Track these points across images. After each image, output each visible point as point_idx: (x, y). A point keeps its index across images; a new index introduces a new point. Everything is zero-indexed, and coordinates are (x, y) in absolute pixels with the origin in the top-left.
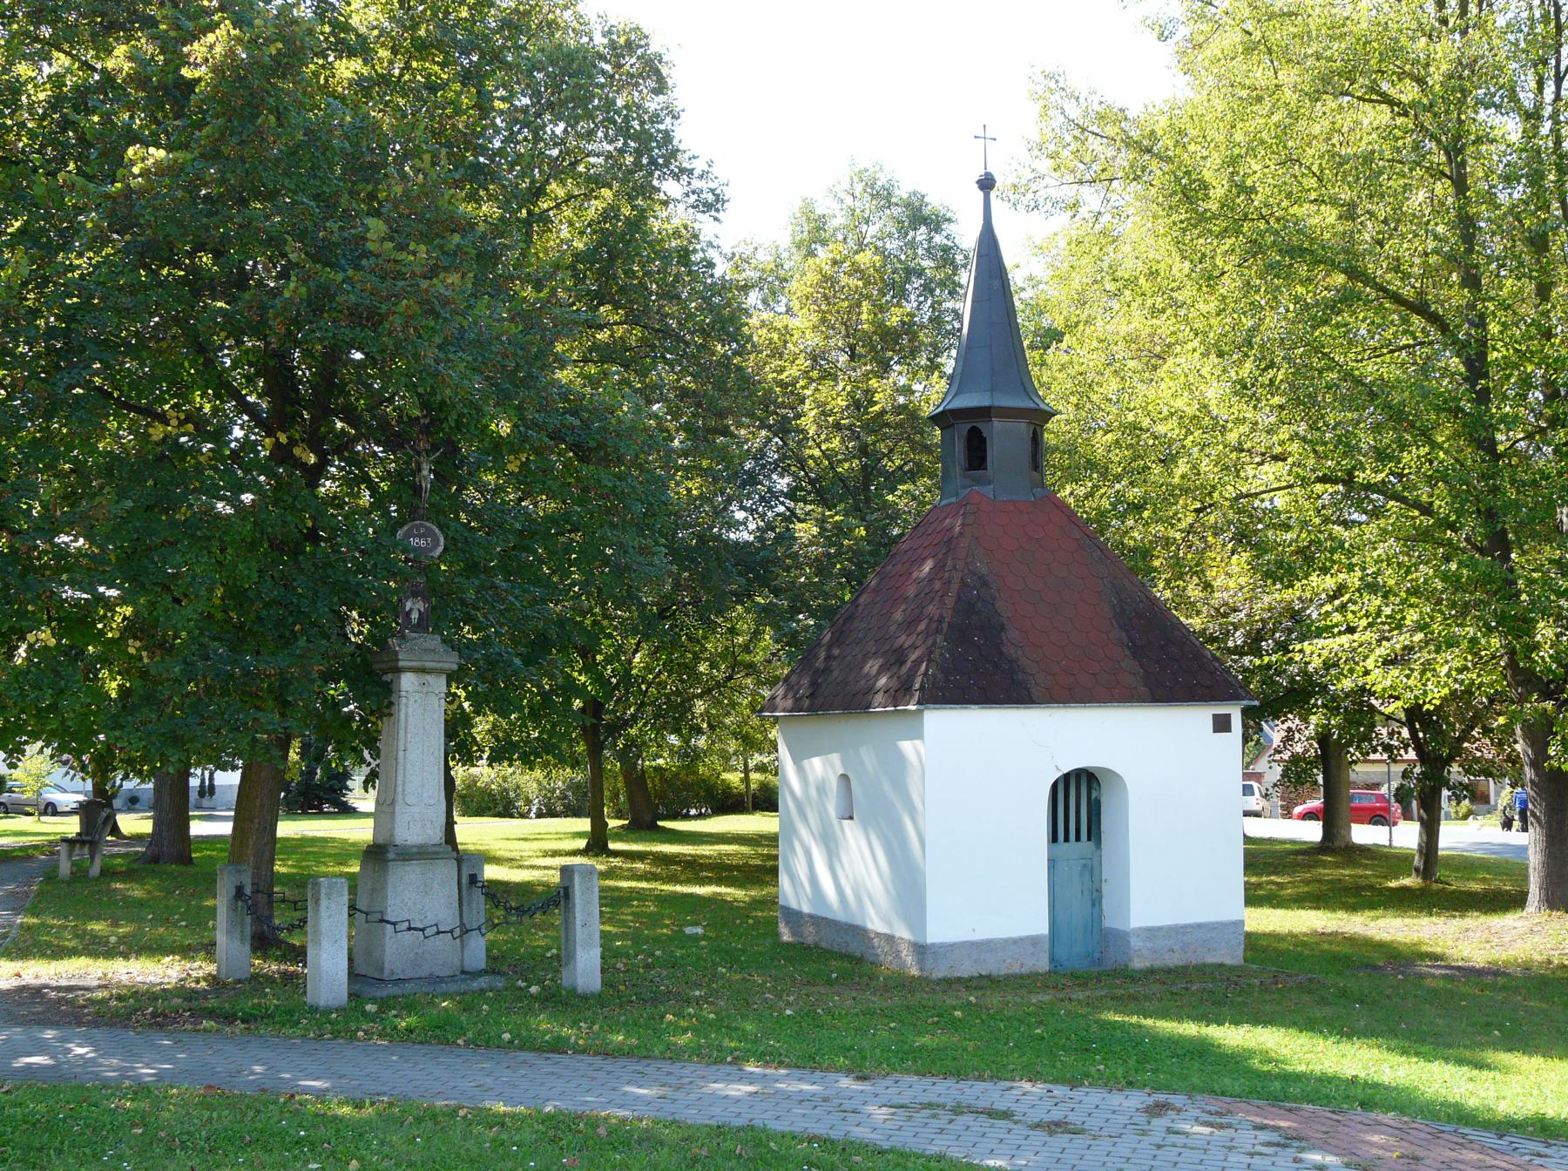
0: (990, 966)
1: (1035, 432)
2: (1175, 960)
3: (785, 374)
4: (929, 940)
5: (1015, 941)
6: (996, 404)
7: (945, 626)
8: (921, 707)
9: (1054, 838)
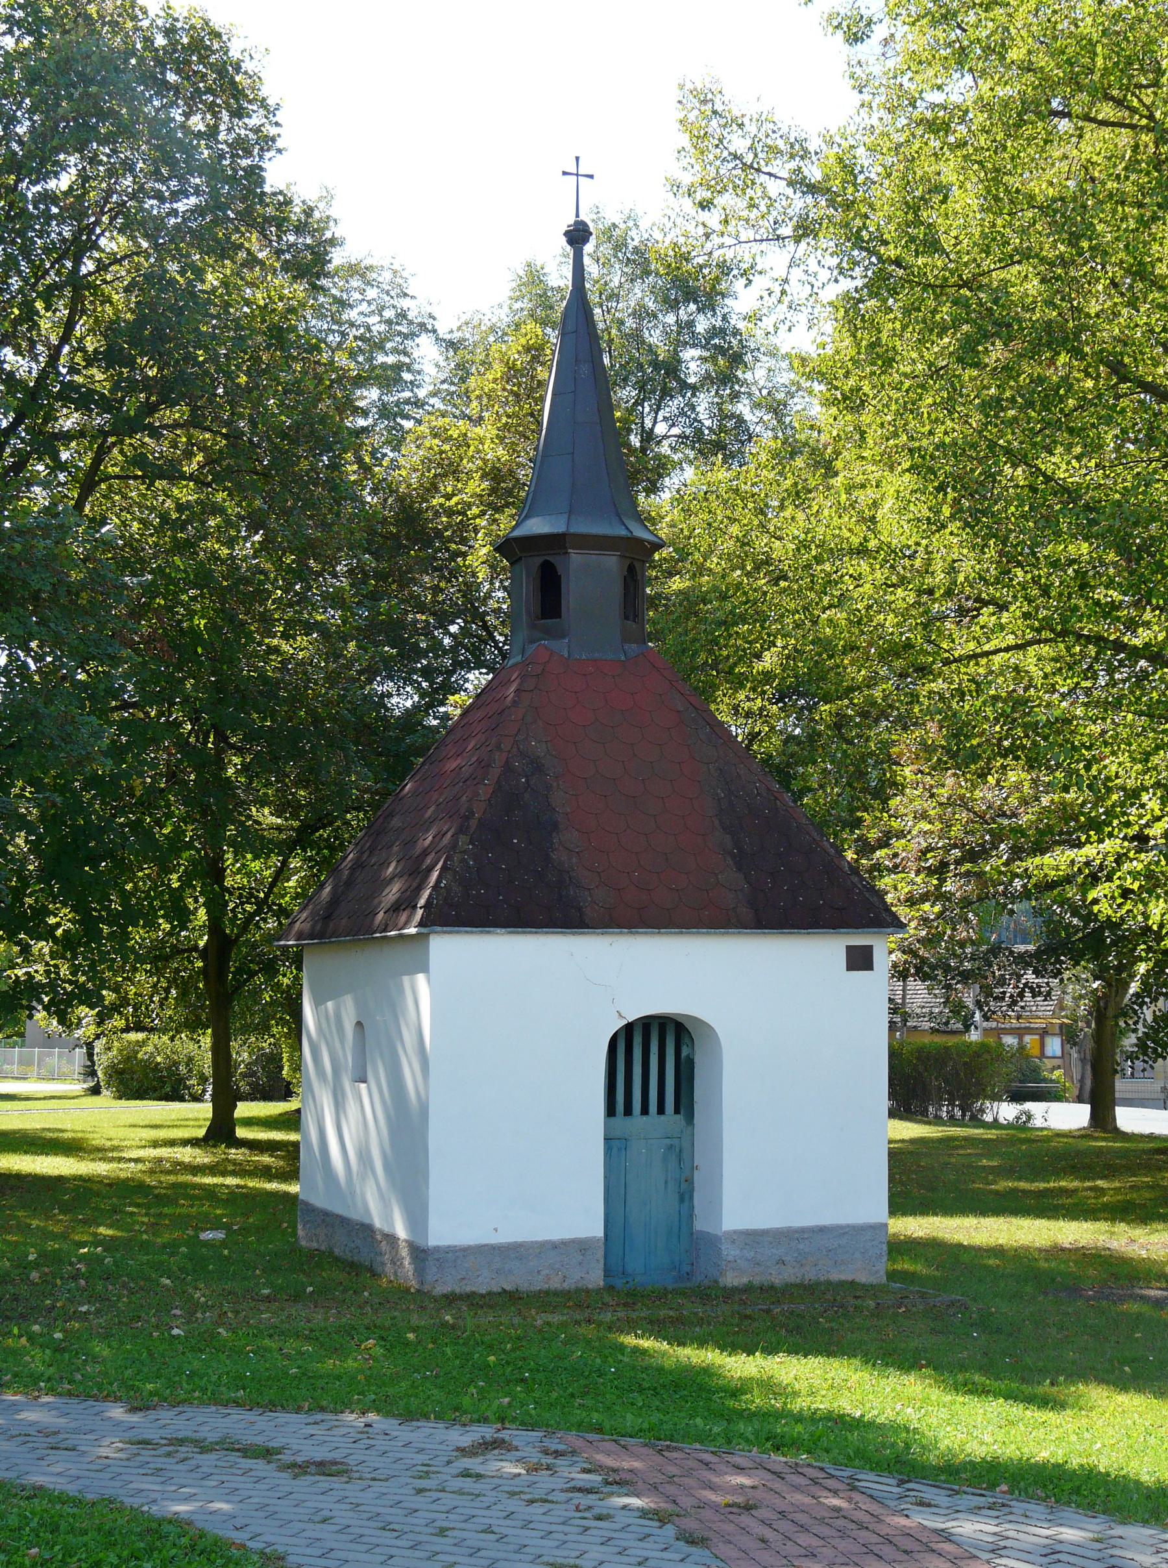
0: (518, 1279)
1: (631, 569)
2: (779, 1277)
3: (455, 500)
4: (433, 1242)
5: (555, 1246)
6: (572, 531)
7: (473, 823)
8: (424, 930)
9: (610, 1111)
